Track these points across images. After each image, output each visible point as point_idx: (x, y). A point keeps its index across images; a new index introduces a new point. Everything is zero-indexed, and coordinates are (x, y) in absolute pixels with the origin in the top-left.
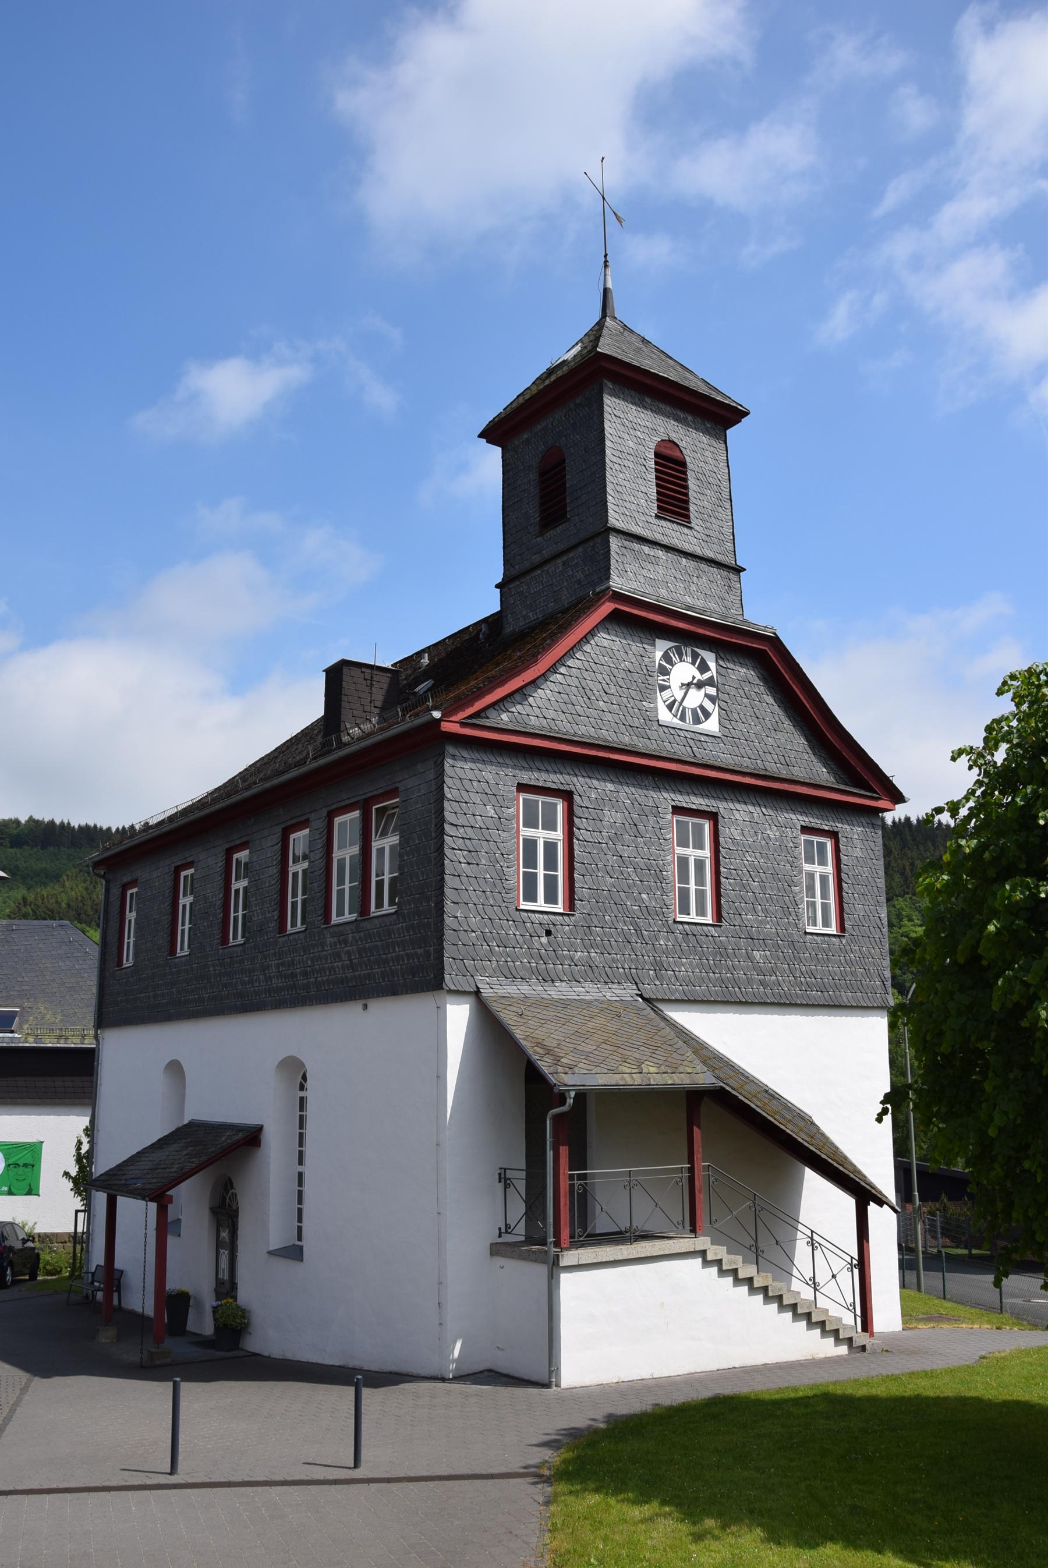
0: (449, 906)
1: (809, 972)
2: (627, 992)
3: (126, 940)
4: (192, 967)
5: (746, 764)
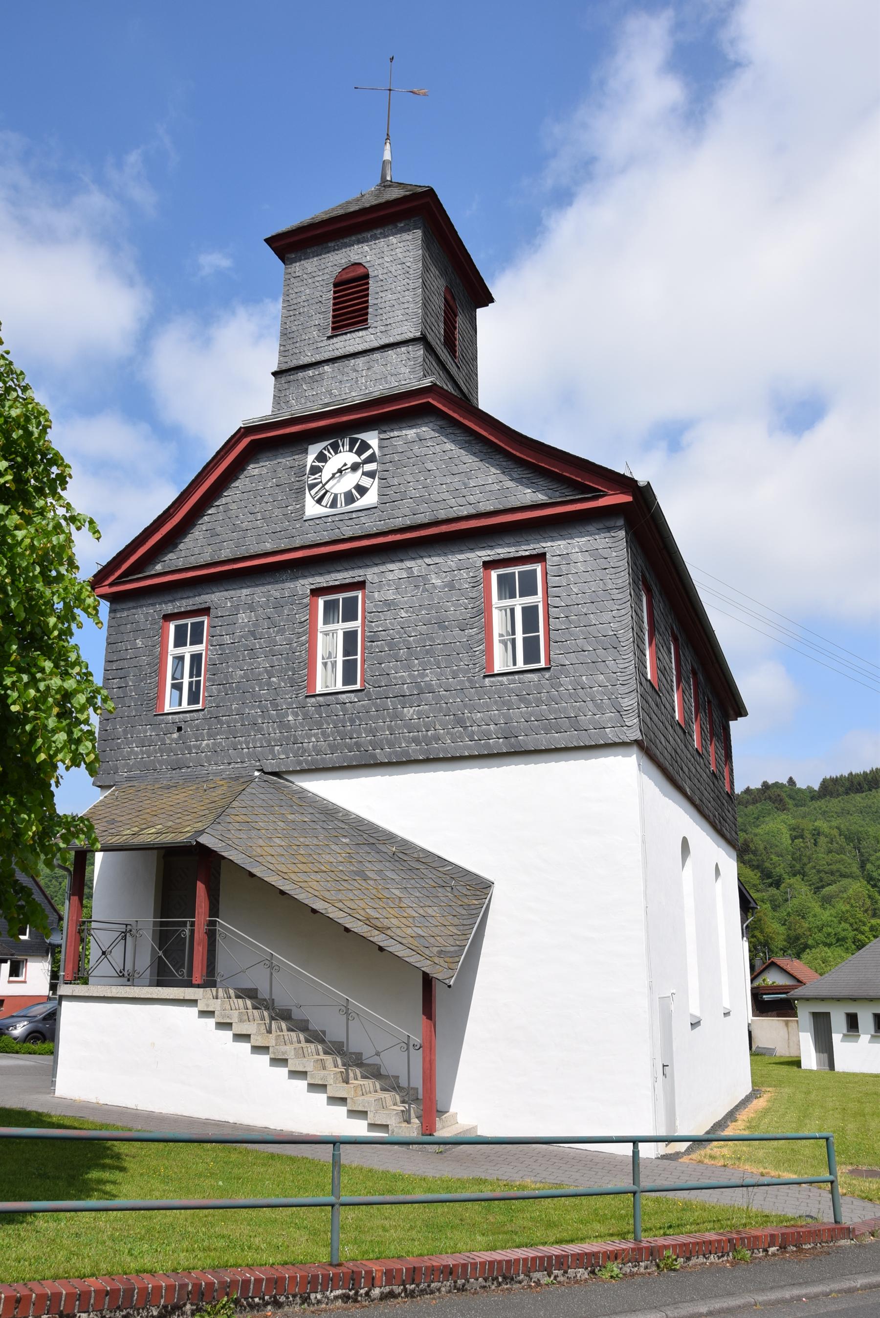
5: (326, 537)
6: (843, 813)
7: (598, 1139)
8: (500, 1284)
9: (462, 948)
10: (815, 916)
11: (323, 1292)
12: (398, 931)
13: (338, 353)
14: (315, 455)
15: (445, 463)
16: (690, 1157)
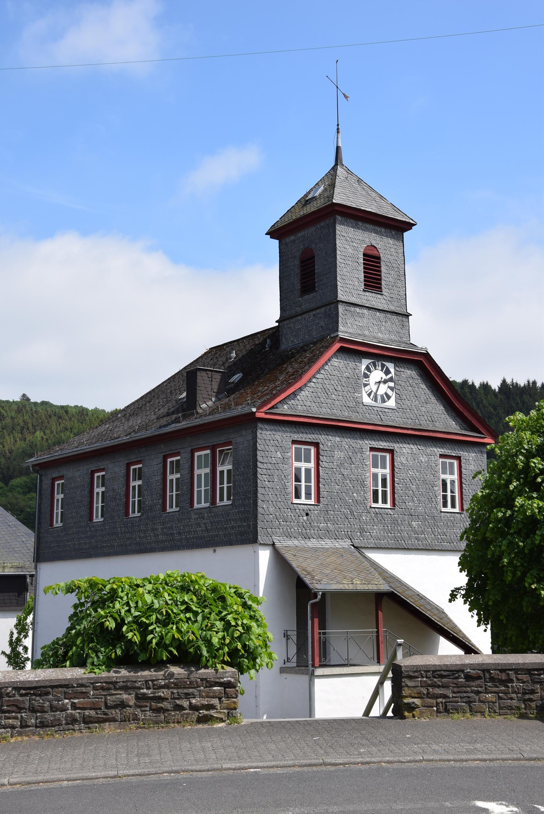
0: (260, 502)
1: (443, 532)
2: (346, 543)
3: (55, 511)
4: (105, 528)
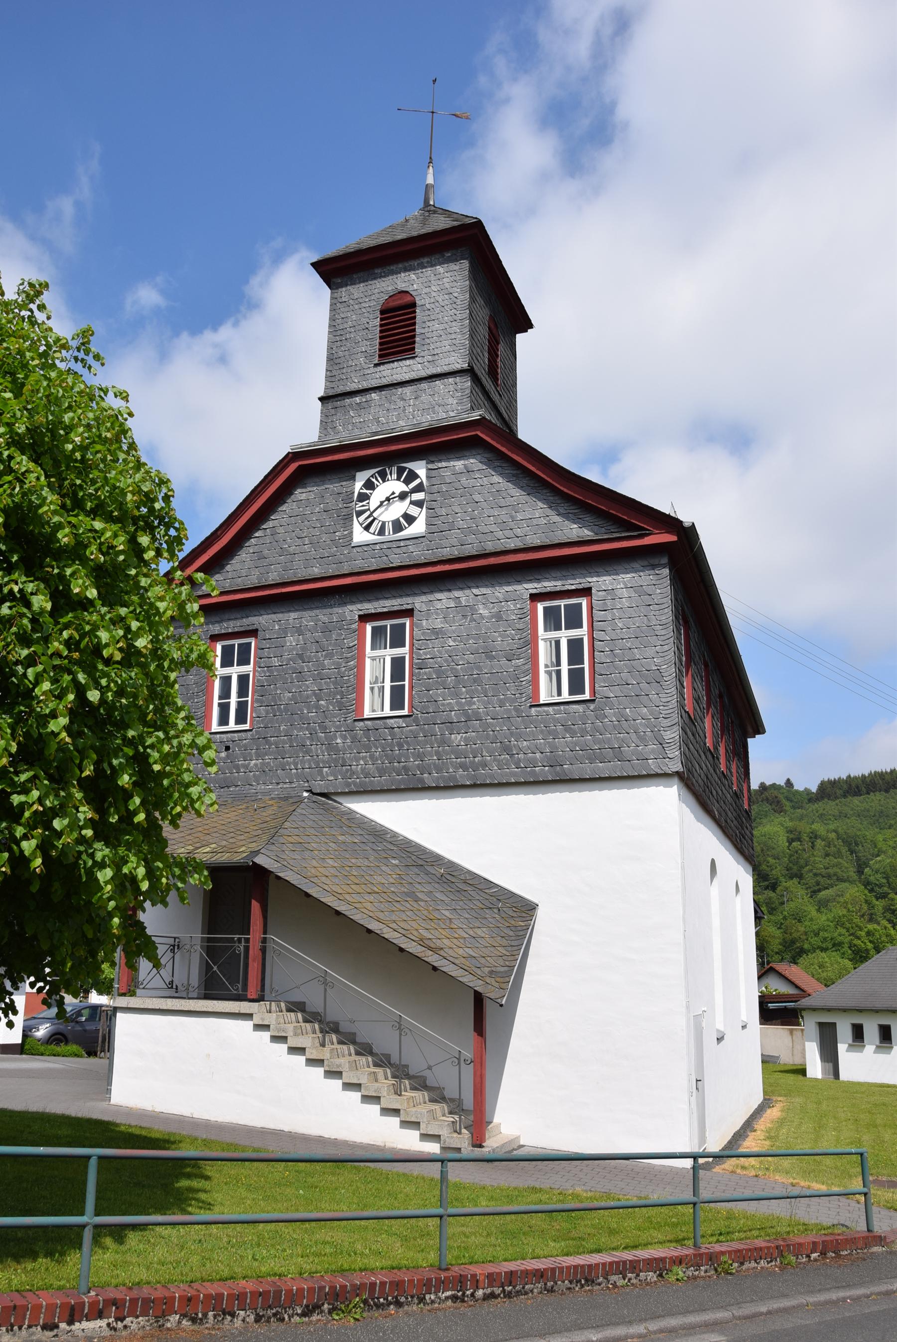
5: (374, 564)
6: (840, 817)
7: (664, 1155)
8: (582, 1286)
9: (512, 968)
10: (811, 920)
11: (436, 1293)
12: (450, 952)
13: (385, 381)
14: (362, 483)
15: (492, 496)
16: (723, 1166)
